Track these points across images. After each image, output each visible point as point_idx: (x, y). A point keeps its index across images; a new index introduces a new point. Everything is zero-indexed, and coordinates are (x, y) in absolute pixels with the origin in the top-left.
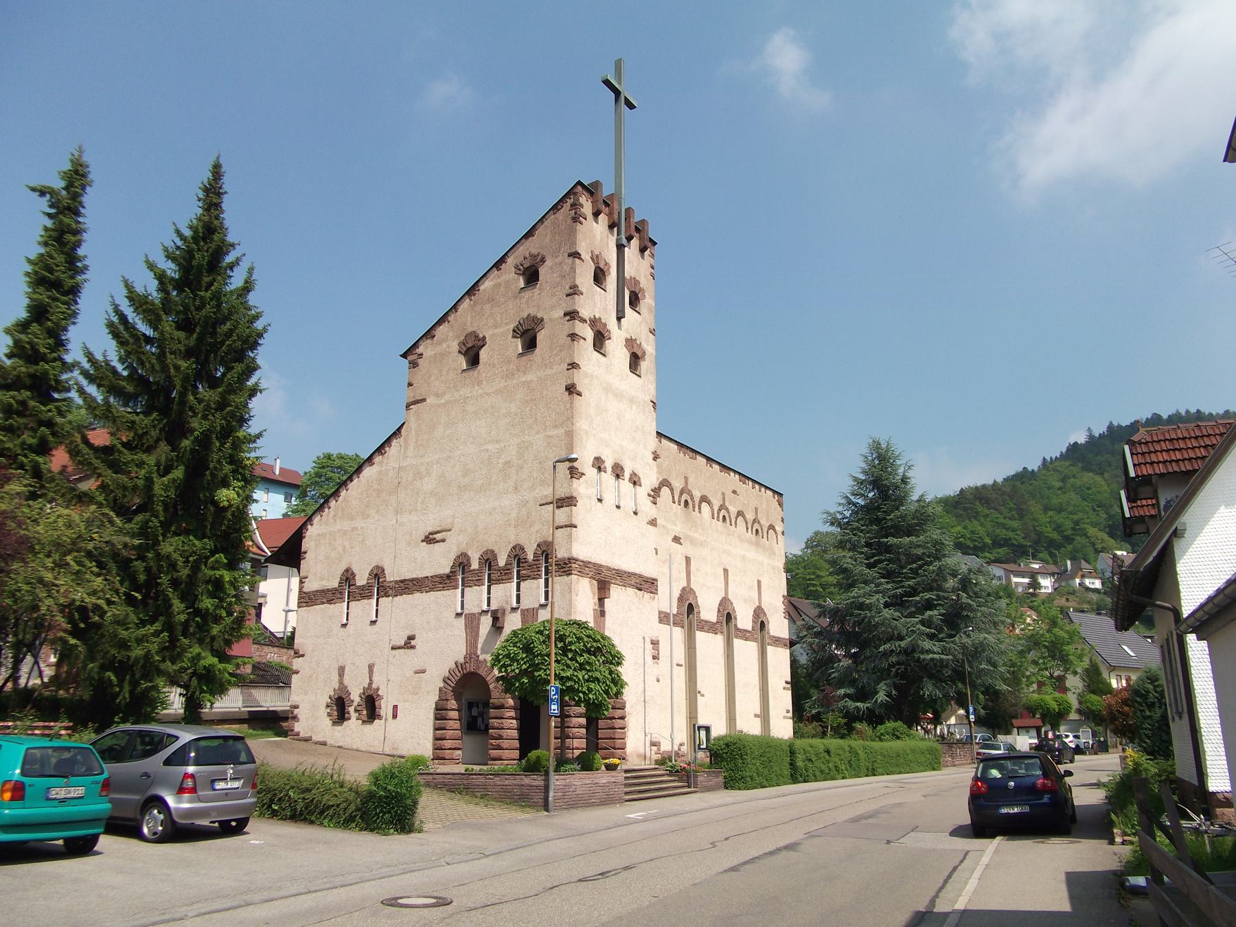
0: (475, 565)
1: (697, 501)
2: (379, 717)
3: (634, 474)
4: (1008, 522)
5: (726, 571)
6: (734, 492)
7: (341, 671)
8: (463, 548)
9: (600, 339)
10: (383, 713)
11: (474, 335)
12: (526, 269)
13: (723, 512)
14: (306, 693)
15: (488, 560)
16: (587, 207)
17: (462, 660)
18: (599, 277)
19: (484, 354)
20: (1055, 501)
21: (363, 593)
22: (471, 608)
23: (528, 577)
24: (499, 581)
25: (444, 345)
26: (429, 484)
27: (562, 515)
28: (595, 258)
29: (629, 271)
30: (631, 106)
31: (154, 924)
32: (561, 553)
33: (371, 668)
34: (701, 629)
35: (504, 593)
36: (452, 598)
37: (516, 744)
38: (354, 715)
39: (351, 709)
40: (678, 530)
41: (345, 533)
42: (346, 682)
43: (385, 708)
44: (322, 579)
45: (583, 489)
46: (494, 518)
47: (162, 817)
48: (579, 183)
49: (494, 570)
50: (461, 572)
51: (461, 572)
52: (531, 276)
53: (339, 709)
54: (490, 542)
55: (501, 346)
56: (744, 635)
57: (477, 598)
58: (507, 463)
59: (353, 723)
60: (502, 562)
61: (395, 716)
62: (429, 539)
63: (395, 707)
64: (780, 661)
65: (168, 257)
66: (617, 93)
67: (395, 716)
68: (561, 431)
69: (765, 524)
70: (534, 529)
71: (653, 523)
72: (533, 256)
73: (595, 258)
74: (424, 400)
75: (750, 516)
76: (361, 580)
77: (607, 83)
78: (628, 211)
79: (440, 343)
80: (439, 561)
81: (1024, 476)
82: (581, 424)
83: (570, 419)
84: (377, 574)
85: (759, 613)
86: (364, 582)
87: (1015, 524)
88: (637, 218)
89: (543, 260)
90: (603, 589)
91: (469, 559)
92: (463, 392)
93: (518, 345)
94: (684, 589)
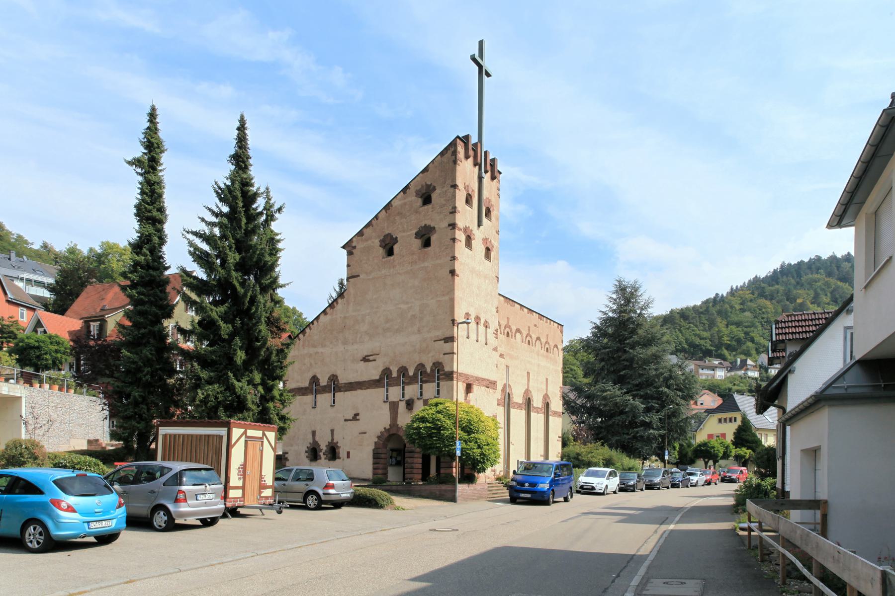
0: (395, 375)
1: (514, 331)
2: (339, 458)
3: (486, 322)
4: (702, 333)
5: (528, 373)
6: (535, 325)
7: (314, 433)
8: (387, 365)
9: (469, 239)
10: (341, 456)
11: (389, 236)
12: (423, 194)
13: (528, 338)
14: (292, 445)
15: (403, 371)
16: (461, 149)
17: (388, 427)
18: (468, 200)
19: (396, 248)
20: (735, 318)
21: (325, 390)
22: (392, 398)
23: (426, 382)
24: (409, 384)
25: (370, 242)
26: (364, 328)
27: (446, 347)
28: (466, 188)
29: (485, 194)
30: (488, 75)
31: (80, 593)
32: (447, 369)
33: (332, 431)
34: (514, 407)
35: (412, 391)
36: (380, 392)
37: (420, 471)
38: (323, 457)
39: (321, 454)
40: (501, 350)
41: (310, 356)
42: (317, 439)
43: (342, 453)
44: (298, 382)
45: (460, 332)
46: (404, 348)
47: (166, 518)
48: (458, 137)
49: (404, 377)
50: (385, 379)
51: (385, 379)
52: (427, 200)
53: (314, 454)
54: (404, 362)
55: (407, 243)
56: (537, 410)
57: (395, 393)
58: (414, 316)
59: (323, 460)
60: (411, 373)
61: (348, 456)
62: (365, 359)
63: (348, 453)
64: (558, 426)
65: (221, 200)
66: (480, 67)
67: (348, 456)
68: (447, 298)
69: (552, 344)
70: (431, 354)
71: (495, 349)
72: (428, 186)
73: (466, 188)
74: (358, 276)
75: (543, 340)
76: (323, 382)
77: (473, 59)
78: (486, 152)
79: (367, 240)
80: (373, 372)
81: (717, 301)
82: (458, 294)
83: (451, 290)
84: (334, 378)
85: (546, 396)
86: (325, 384)
87: (705, 334)
88: (491, 157)
89: (434, 189)
90: (469, 388)
91: (391, 371)
92: (383, 272)
93: (418, 243)
94: (505, 385)
